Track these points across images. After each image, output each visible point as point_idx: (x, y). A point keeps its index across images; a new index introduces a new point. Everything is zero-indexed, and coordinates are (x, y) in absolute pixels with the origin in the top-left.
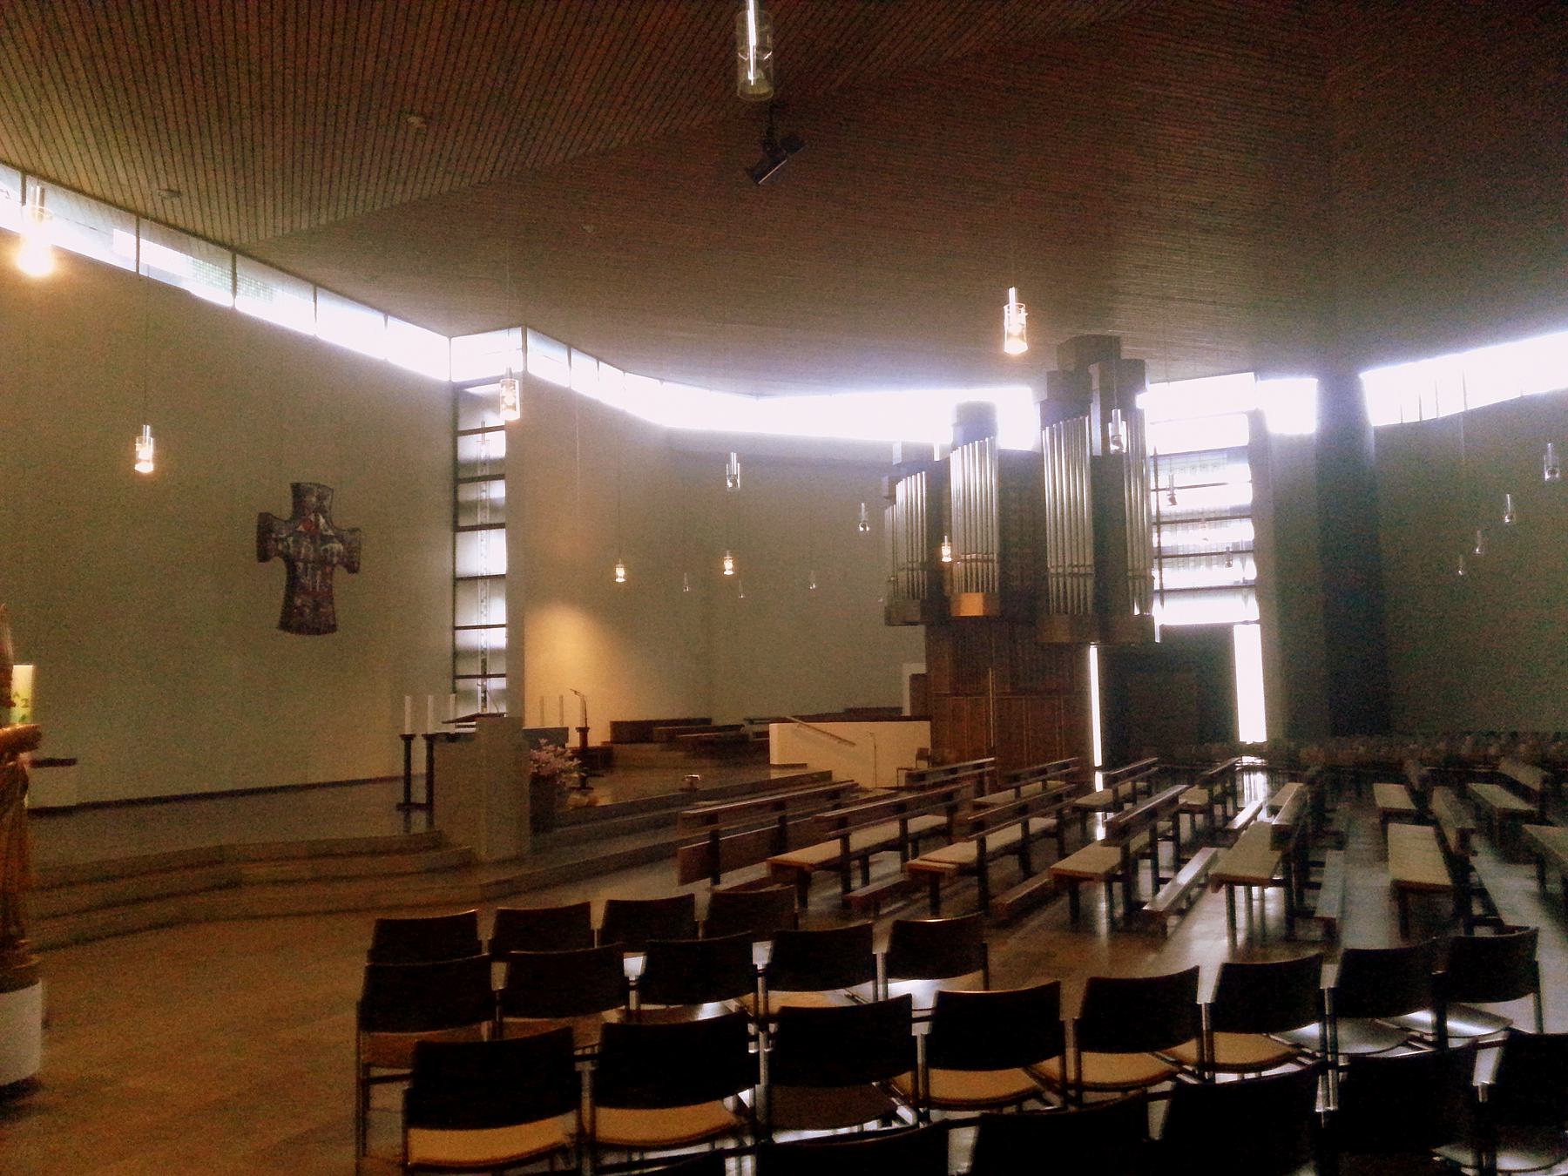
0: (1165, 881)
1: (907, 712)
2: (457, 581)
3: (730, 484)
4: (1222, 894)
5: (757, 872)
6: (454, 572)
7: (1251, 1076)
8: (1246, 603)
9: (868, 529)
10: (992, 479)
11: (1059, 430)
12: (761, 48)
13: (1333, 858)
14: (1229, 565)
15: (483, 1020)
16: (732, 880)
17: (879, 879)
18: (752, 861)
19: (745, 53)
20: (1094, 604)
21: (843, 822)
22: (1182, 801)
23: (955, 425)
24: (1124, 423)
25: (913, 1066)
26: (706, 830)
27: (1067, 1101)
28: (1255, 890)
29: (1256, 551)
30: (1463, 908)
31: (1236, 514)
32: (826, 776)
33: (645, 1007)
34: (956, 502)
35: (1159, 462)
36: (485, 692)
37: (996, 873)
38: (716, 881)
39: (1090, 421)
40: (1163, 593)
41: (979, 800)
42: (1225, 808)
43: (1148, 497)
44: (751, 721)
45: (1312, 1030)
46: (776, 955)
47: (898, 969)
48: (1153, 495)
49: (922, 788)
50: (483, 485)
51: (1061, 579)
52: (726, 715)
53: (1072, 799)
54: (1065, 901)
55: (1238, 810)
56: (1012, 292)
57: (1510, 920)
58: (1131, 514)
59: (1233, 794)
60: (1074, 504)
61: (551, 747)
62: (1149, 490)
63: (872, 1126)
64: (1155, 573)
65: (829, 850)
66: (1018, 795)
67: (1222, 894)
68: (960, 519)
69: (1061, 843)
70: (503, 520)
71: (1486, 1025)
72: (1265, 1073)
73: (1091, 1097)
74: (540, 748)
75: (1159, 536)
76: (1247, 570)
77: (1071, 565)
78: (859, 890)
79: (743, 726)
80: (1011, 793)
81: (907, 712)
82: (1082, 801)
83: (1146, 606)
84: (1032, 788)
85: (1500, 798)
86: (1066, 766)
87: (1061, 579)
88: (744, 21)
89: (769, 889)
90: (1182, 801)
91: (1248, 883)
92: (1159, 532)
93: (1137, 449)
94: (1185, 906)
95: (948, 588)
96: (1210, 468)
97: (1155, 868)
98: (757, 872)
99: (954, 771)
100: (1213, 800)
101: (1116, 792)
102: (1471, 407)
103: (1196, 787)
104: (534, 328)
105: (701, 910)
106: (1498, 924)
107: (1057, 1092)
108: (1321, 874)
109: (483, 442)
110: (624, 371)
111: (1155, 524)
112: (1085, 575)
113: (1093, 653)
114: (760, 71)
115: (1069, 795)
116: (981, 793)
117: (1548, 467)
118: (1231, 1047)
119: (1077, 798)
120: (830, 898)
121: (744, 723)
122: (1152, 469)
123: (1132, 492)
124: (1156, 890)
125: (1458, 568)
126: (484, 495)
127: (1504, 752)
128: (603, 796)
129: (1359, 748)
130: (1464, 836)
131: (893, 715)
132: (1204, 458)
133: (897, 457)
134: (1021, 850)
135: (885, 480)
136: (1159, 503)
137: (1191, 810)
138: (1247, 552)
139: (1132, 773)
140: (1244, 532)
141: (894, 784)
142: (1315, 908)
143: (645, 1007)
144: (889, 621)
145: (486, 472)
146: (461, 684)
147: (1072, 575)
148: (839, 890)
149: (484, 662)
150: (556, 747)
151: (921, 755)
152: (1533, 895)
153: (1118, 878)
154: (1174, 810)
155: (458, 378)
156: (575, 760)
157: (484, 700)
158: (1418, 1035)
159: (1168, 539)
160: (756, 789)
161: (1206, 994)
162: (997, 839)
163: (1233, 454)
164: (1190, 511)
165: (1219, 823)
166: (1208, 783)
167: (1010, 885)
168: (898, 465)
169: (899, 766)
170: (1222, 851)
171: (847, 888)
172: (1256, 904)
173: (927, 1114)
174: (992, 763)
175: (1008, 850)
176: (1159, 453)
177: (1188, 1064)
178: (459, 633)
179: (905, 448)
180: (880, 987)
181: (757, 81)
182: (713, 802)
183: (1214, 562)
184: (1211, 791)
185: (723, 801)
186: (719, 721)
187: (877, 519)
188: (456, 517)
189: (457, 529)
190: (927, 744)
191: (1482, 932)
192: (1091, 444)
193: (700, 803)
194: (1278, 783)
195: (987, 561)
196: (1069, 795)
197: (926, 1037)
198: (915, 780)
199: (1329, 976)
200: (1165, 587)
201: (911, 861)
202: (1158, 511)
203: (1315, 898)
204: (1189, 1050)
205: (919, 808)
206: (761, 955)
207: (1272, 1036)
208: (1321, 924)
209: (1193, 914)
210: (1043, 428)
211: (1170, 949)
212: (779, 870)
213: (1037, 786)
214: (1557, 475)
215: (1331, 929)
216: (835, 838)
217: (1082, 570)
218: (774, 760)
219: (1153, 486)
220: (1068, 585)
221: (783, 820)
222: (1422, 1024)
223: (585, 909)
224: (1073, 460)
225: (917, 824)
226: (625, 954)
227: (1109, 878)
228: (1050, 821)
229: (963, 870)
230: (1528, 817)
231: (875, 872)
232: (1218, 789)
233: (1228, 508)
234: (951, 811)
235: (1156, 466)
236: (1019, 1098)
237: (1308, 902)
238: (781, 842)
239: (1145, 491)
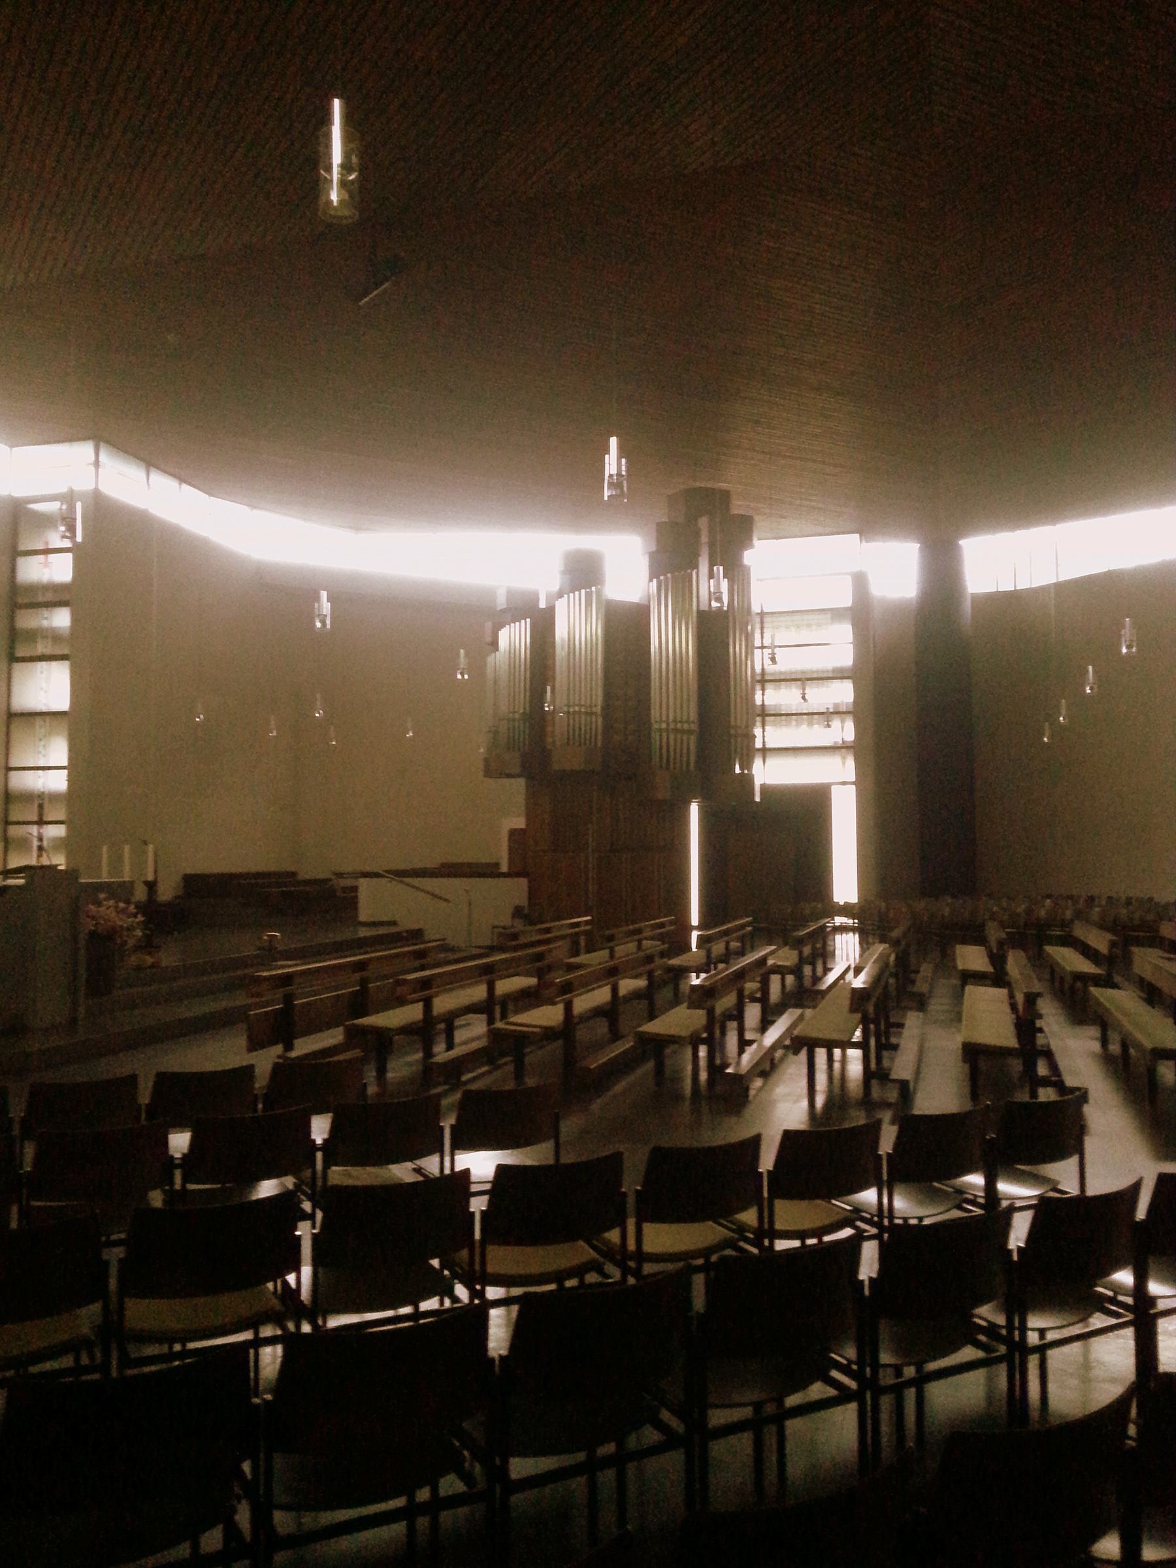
0: (750, 1043)
1: (504, 868)
2: (14, 717)
3: (318, 625)
4: (803, 1055)
5: (333, 1037)
6: (9, 705)
7: (811, 1241)
8: (844, 763)
9: (466, 677)
10: (596, 628)
11: (667, 579)
12: (346, 167)
13: (913, 1021)
14: (829, 726)
16: (304, 1046)
17: (465, 1043)
18: (329, 1026)
19: (329, 168)
20: (696, 762)
21: (426, 984)
22: (770, 962)
23: (564, 573)
24: (726, 580)
25: (101, 1293)
26: (279, 994)
27: (626, 1272)
28: (837, 1052)
29: (856, 712)
30: (1030, 1067)
31: (838, 675)
32: (416, 935)
33: (192, 1187)
34: (560, 652)
35: (765, 620)
36: (40, 839)
37: (582, 1034)
38: (289, 1047)
39: (698, 576)
40: (765, 751)
41: (572, 960)
42: (814, 970)
43: (753, 653)
44: (340, 875)
45: (869, 1196)
46: (334, 1130)
47: (467, 1140)
48: (757, 652)
49: (515, 949)
50: (45, 612)
51: (664, 734)
52: (311, 870)
53: (665, 960)
54: (650, 1065)
55: (827, 970)
56: (613, 441)
57: (1070, 1081)
58: (735, 671)
59: (823, 955)
60: (679, 659)
61: (111, 902)
62: (754, 647)
63: (430, 1304)
64: (758, 731)
65: (412, 1013)
66: (612, 956)
67: (803, 1055)
68: (565, 668)
69: (651, 1004)
70: (66, 651)
71: (1033, 1186)
72: (826, 1239)
73: (648, 1268)
74: (99, 904)
75: (763, 695)
76: (846, 731)
77: (675, 721)
78: (441, 1054)
79: (330, 880)
80: (605, 953)
81: (504, 868)
82: (675, 962)
83: (747, 764)
84: (626, 949)
85: (1071, 961)
86: (662, 925)
87: (664, 734)
88: (328, 136)
89: (341, 1057)
90: (770, 962)
91: (830, 1045)
92: (763, 690)
93: (743, 604)
94: (767, 1067)
95: (550, 740)
96: (814, 627)
97: (741, 1031)
98: (333, 1037)
99: (548, 930)
100: (802, 960)
101: (709, 952)
102: (1062, 578)
103: (788, 947)
104: (107, 442)
105: (261, 1081)
106: (1060, 1086)
107: (617, 1264)
108: (900, 1034)
109: (46, 564)
110: (210, 494)
111: (758, 681)
112: (690, 732)
113: (694, 809)
114: (343, 192)
115: (662, 955)
116: (576, 953)
117: (1126, 641)
118: (788, 1213)
119: (670, 959)
120: (410, 1064)
121: (333, 877)
122: (758, 626)
123: (737, 647)
124: (741, 1051)
125: (1044, 735)
126: (45, 623)
127: (1079, 915)
128: (168, 958)
129: (946, 907)
130: (1031, 999)
131: (488, 871)
132: (796, 617)
133: (501, 602)
134: (609, 1013)
135: (489, 625)
136: (759, 661)
137: (779, 970)
139: (726, 933)
140: (844, 693)
141: (488, 943)
142: (890, 1070)
143: (192, 1187)
144: (489, 773)
145: (49, 597)
146: (13, 831)
147: (676, 730)
148: (420, 1055)
149: (41, 807)
150: (117, 902)
151: (518, 912)
152: (1093, 1055)
153: (703, 1041)
154: (762, 971)
155: (19, 493)
156: (139, 916)
157: (40, 848)
158: (971, 1197)
159: (772, 697)
160: (339, 948)
161: (767, 1161)
162: (583, 1003)
163: (836, 614)
164: (793, 670)
165: (807, 982)
166: (798, 944)
167: (599, 1046)
168: (503, 611)
169: (496, 923)
170: (809, 1012)
171: (428, 1054)
172: (837, 1066)
173: (483, 1292)
174: (587, 922)
175: (598, 1012)
176: (765, 611)
177: (749, 1232)
178: (12, 774)
179: (510, 594)
180: (447, 1160)
181: (341, 202)
182: (290, 963)
183: (815, 721)
184: (801, 953)
185: (298, 962)
186: (305, 874)
187: (477, 667)
188: (12, 647)
189: (13, 659)
190: (524, 902)
191: (1046, 1095)
192: (698, 597)
193: (280, 963)
194: (868, 943)
195: (592, 714)
196: (662, 955)
197: (120, 1261)
198: (506, 940)
199: (887, 1143)
200: (768, 746)
201: (499, 1025)
202: (763, 669)
203: (892, 1059)
204: (749, 1217)
205: (510, 968)
206: (320, 1129)
207: (834, 1202)
208: (898, 1086)
209: (774, 1077)
210: (651, 580)
211: (748, 1112)
212: (355, 1036)
213: (632, 946)
214: (1134, 650)
215: (906, 1091)
216: (418, 1001)
217: (686, 726)
218: (363, 917)
219: (757, 643)
221: (364, 982)
222: (974, 1186)
223: (132, 1080)
224: (680, 613)
225: (506, 986)
226: (171, 1129)
227: (695, 1042)
228: (642, 983)
229: (549, 1034)
230: (1097, 981)
231: (460, 1036)
232: (807, 950)
234: (540, 973)
235: (762, 623)
236: (579, 1271)
237: (886, 1063)
238: (360, 1004)
239: (750, 647)
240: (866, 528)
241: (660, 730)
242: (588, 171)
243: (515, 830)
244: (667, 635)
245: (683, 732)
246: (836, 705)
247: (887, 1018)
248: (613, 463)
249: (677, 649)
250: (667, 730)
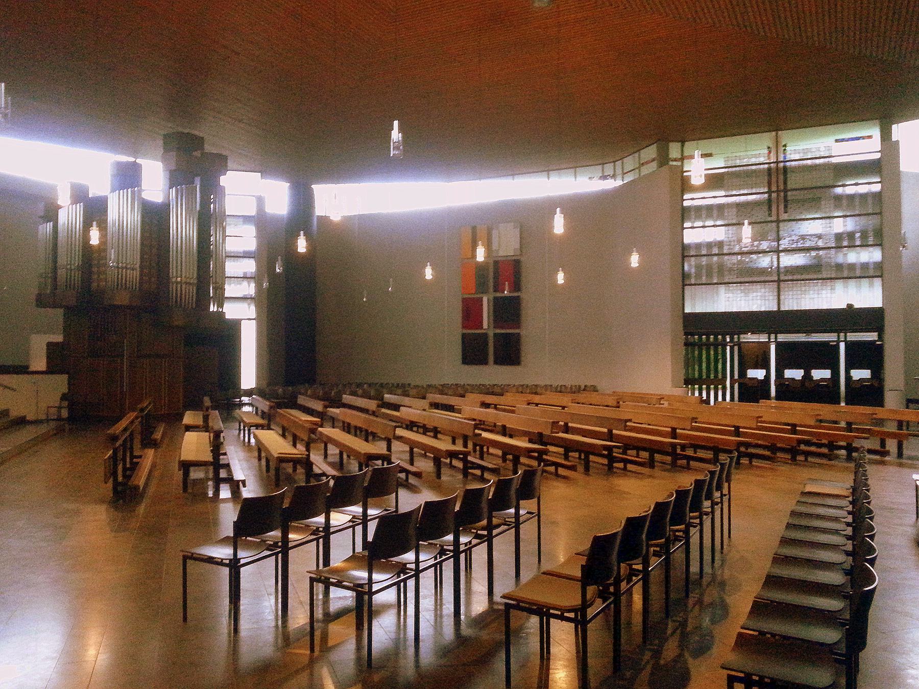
15: (282, 534)
29: (256, 278)
30: (216, 473)
31: (246, 255)
56: (396, 123)
138: (251, 278)
147: (186, 283)
210: (171, 187)
220: (183, 289)
233: (242, 251)
240: (265, 170)
241: (177, 283)
242: (861, 41)
243: (51, 343)
244: (182, 224)
245: (190, 284)
246: (245, 273)
247: (131, 453)
248: (396, 135)
249: (188, 236)
250: (181, 282)
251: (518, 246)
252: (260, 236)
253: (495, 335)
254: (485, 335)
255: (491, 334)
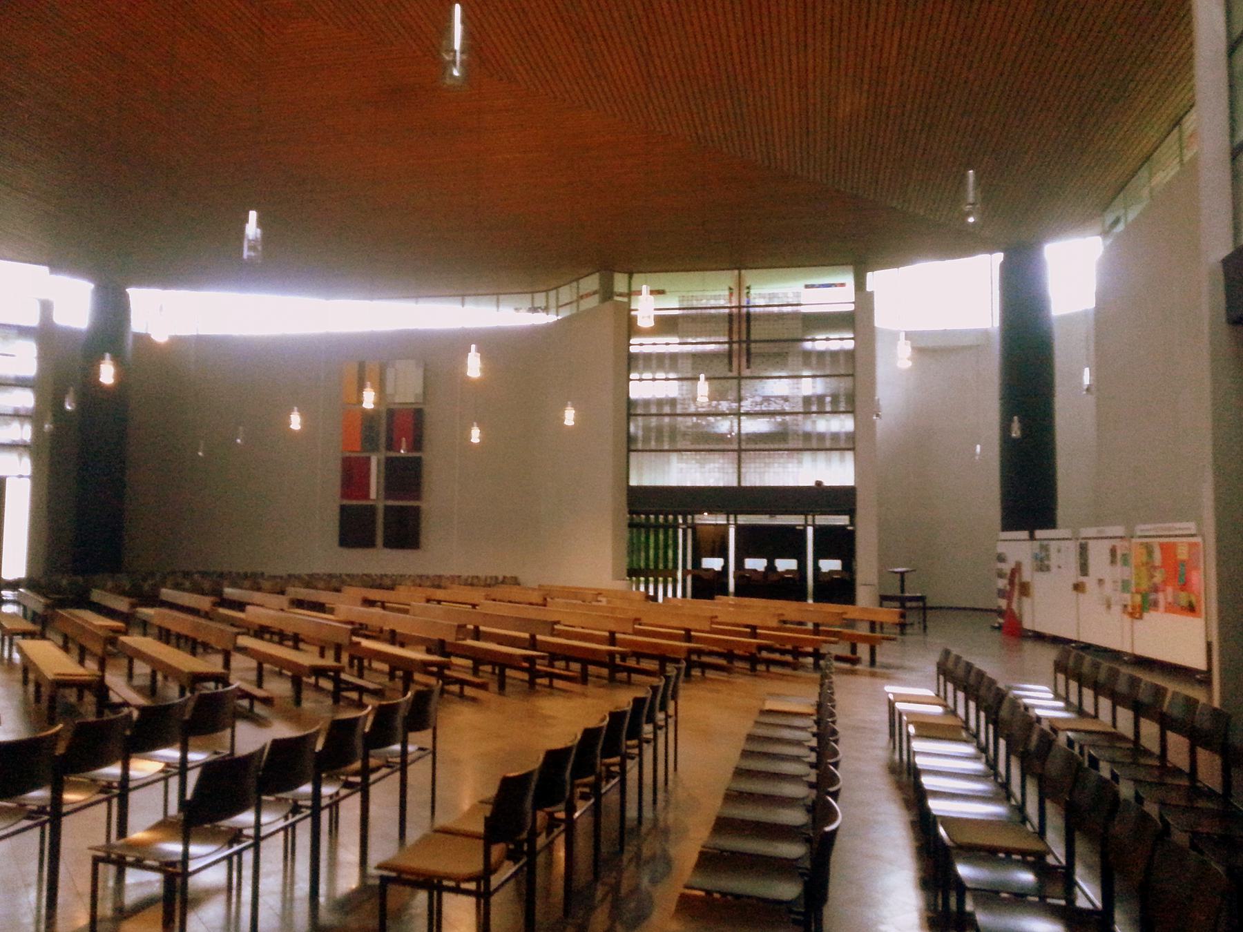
29: (34, 417)
163: (23, 332)
240: (56, 265)
251: (419, 390)
252: (44, 356)
253: (387, 508)
254: (372, 510)
255: (380, 506)
